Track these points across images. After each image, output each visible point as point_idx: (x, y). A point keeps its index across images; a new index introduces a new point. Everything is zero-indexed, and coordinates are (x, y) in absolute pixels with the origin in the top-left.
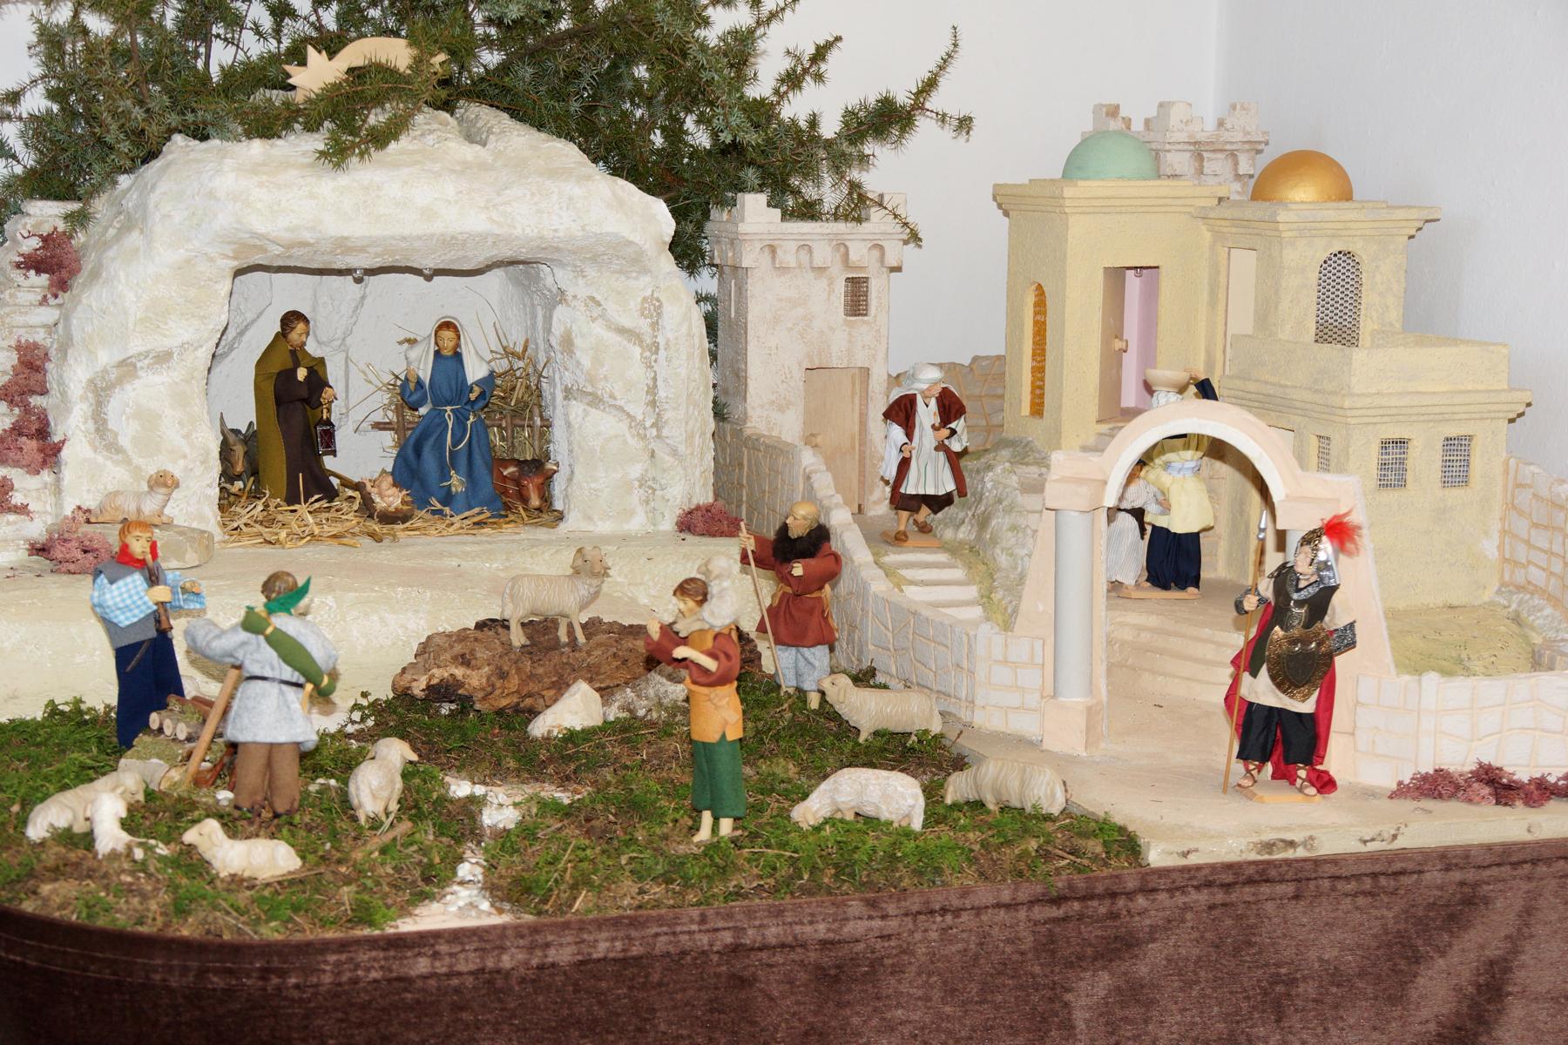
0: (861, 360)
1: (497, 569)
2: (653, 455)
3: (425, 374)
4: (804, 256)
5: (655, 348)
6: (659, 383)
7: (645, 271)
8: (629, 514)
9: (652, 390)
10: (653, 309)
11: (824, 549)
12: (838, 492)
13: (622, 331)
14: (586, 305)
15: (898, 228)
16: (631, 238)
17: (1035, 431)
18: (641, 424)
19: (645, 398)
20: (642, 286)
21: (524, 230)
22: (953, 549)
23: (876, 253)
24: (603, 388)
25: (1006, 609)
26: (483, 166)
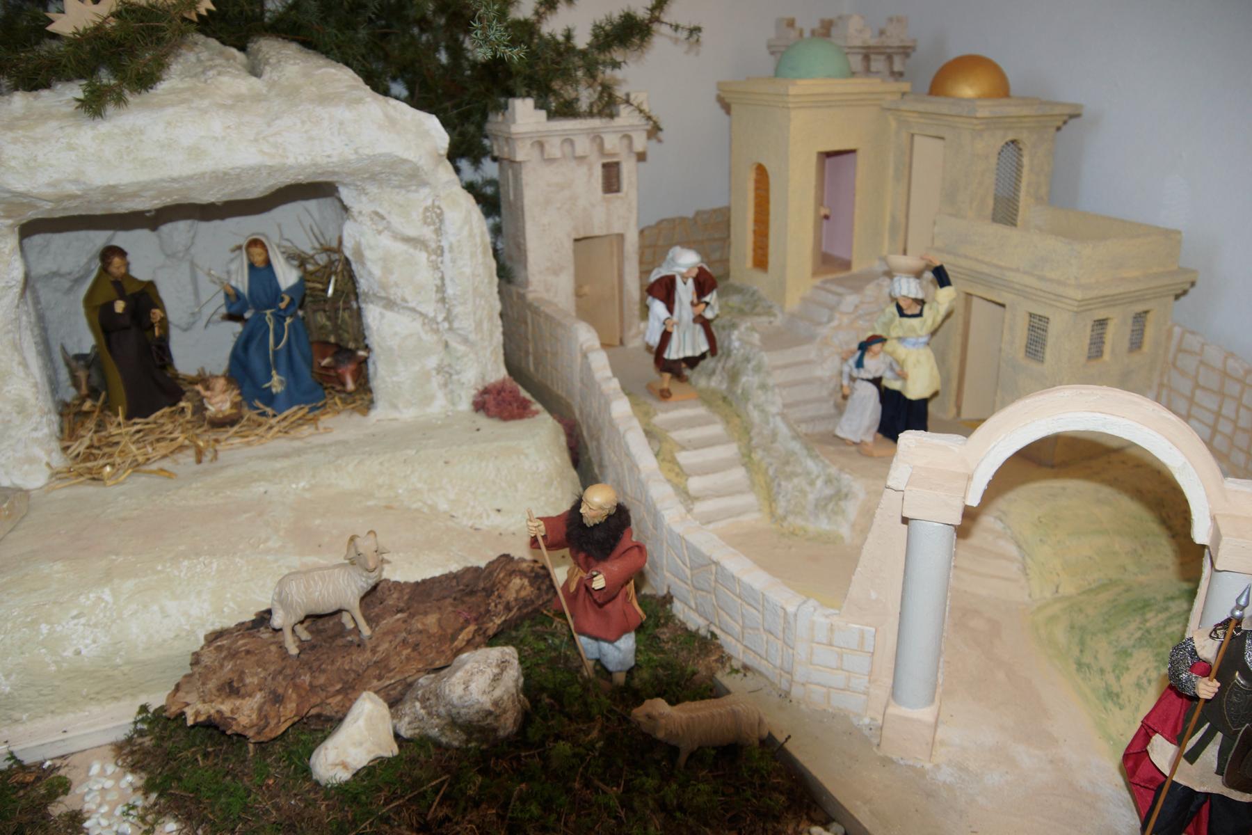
0: (617, 229)
1: (304, 489)
2: (447, 345)
3: (243, 286)
4: (567, 148)
5: (440, 251)
6: (447, 281)
7: (424, 184)
8: (428, 399)
9: (441, 289)
10: (435, 217)
11: (624, 543)
12: (615, 374)
13: (407, 240)
14: (372, 219)
15: (643, 121)
16: (405, 155)
17: (759, 282)
18: (434, 320)
19: (434, 296)
20: (423, 197)
21: (296, 159)
22: (707, 398)
23: (625, 142)
24: (395, 294)
25: (767, 470)
26: (257, 98)
